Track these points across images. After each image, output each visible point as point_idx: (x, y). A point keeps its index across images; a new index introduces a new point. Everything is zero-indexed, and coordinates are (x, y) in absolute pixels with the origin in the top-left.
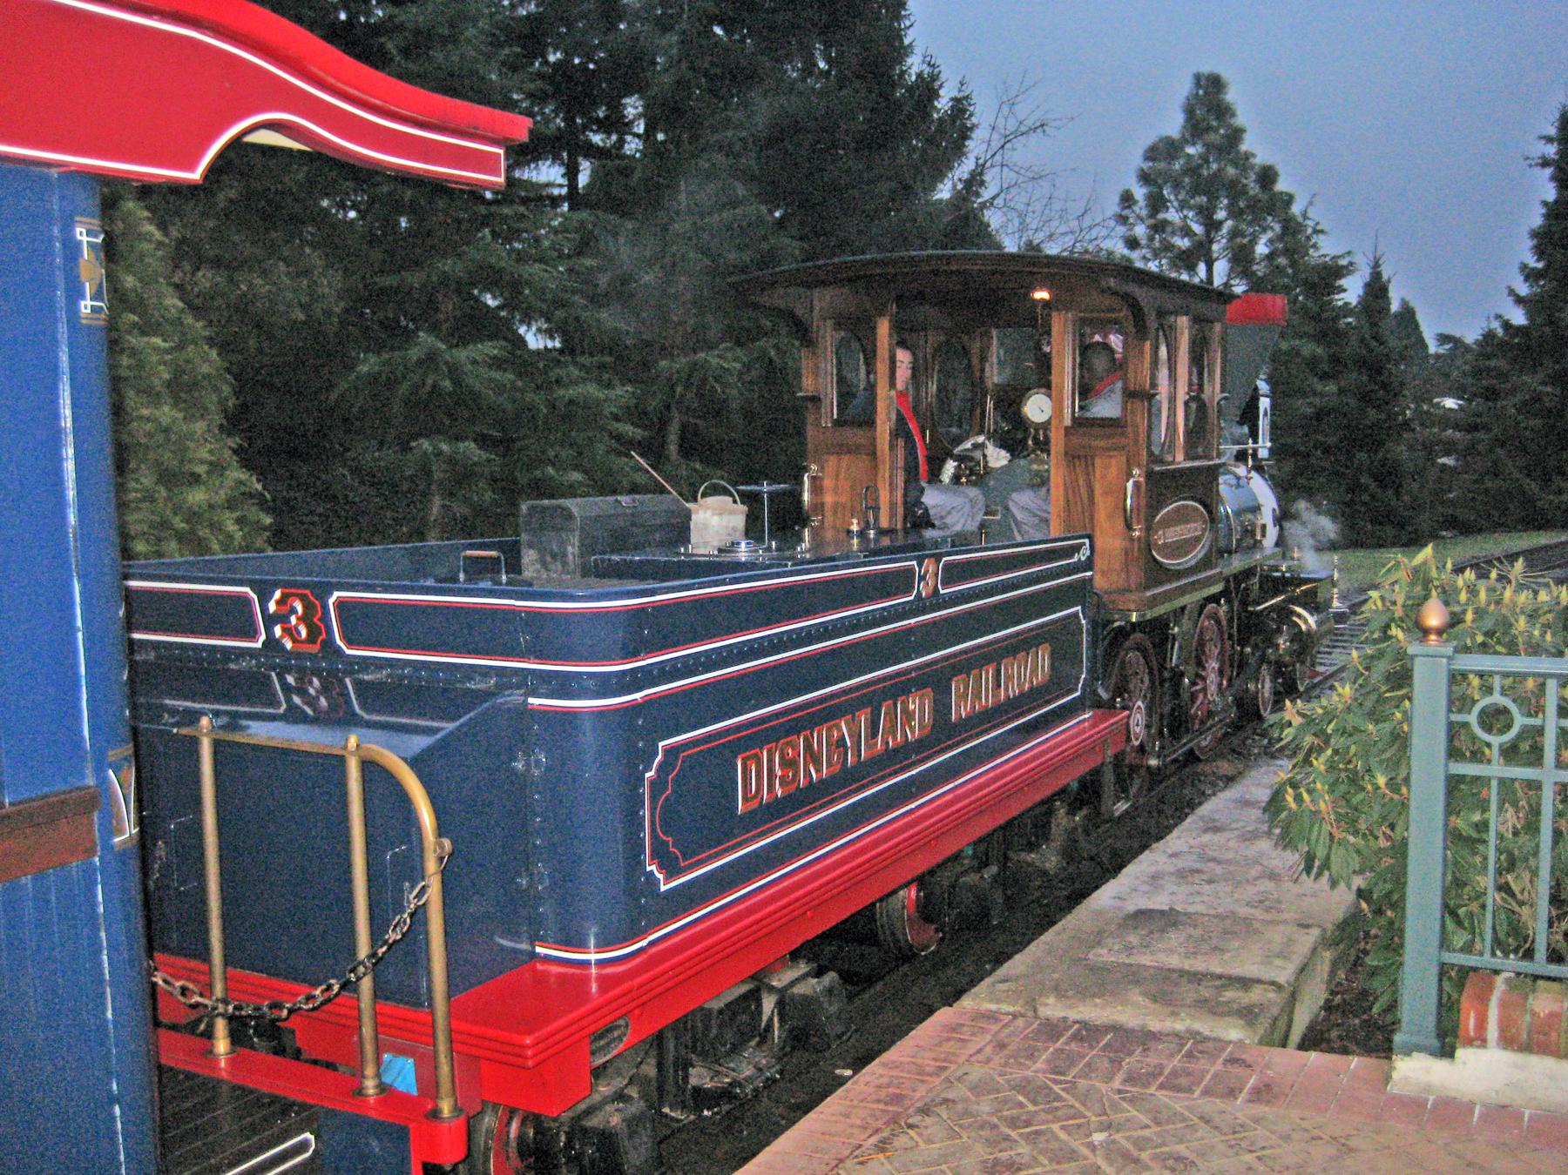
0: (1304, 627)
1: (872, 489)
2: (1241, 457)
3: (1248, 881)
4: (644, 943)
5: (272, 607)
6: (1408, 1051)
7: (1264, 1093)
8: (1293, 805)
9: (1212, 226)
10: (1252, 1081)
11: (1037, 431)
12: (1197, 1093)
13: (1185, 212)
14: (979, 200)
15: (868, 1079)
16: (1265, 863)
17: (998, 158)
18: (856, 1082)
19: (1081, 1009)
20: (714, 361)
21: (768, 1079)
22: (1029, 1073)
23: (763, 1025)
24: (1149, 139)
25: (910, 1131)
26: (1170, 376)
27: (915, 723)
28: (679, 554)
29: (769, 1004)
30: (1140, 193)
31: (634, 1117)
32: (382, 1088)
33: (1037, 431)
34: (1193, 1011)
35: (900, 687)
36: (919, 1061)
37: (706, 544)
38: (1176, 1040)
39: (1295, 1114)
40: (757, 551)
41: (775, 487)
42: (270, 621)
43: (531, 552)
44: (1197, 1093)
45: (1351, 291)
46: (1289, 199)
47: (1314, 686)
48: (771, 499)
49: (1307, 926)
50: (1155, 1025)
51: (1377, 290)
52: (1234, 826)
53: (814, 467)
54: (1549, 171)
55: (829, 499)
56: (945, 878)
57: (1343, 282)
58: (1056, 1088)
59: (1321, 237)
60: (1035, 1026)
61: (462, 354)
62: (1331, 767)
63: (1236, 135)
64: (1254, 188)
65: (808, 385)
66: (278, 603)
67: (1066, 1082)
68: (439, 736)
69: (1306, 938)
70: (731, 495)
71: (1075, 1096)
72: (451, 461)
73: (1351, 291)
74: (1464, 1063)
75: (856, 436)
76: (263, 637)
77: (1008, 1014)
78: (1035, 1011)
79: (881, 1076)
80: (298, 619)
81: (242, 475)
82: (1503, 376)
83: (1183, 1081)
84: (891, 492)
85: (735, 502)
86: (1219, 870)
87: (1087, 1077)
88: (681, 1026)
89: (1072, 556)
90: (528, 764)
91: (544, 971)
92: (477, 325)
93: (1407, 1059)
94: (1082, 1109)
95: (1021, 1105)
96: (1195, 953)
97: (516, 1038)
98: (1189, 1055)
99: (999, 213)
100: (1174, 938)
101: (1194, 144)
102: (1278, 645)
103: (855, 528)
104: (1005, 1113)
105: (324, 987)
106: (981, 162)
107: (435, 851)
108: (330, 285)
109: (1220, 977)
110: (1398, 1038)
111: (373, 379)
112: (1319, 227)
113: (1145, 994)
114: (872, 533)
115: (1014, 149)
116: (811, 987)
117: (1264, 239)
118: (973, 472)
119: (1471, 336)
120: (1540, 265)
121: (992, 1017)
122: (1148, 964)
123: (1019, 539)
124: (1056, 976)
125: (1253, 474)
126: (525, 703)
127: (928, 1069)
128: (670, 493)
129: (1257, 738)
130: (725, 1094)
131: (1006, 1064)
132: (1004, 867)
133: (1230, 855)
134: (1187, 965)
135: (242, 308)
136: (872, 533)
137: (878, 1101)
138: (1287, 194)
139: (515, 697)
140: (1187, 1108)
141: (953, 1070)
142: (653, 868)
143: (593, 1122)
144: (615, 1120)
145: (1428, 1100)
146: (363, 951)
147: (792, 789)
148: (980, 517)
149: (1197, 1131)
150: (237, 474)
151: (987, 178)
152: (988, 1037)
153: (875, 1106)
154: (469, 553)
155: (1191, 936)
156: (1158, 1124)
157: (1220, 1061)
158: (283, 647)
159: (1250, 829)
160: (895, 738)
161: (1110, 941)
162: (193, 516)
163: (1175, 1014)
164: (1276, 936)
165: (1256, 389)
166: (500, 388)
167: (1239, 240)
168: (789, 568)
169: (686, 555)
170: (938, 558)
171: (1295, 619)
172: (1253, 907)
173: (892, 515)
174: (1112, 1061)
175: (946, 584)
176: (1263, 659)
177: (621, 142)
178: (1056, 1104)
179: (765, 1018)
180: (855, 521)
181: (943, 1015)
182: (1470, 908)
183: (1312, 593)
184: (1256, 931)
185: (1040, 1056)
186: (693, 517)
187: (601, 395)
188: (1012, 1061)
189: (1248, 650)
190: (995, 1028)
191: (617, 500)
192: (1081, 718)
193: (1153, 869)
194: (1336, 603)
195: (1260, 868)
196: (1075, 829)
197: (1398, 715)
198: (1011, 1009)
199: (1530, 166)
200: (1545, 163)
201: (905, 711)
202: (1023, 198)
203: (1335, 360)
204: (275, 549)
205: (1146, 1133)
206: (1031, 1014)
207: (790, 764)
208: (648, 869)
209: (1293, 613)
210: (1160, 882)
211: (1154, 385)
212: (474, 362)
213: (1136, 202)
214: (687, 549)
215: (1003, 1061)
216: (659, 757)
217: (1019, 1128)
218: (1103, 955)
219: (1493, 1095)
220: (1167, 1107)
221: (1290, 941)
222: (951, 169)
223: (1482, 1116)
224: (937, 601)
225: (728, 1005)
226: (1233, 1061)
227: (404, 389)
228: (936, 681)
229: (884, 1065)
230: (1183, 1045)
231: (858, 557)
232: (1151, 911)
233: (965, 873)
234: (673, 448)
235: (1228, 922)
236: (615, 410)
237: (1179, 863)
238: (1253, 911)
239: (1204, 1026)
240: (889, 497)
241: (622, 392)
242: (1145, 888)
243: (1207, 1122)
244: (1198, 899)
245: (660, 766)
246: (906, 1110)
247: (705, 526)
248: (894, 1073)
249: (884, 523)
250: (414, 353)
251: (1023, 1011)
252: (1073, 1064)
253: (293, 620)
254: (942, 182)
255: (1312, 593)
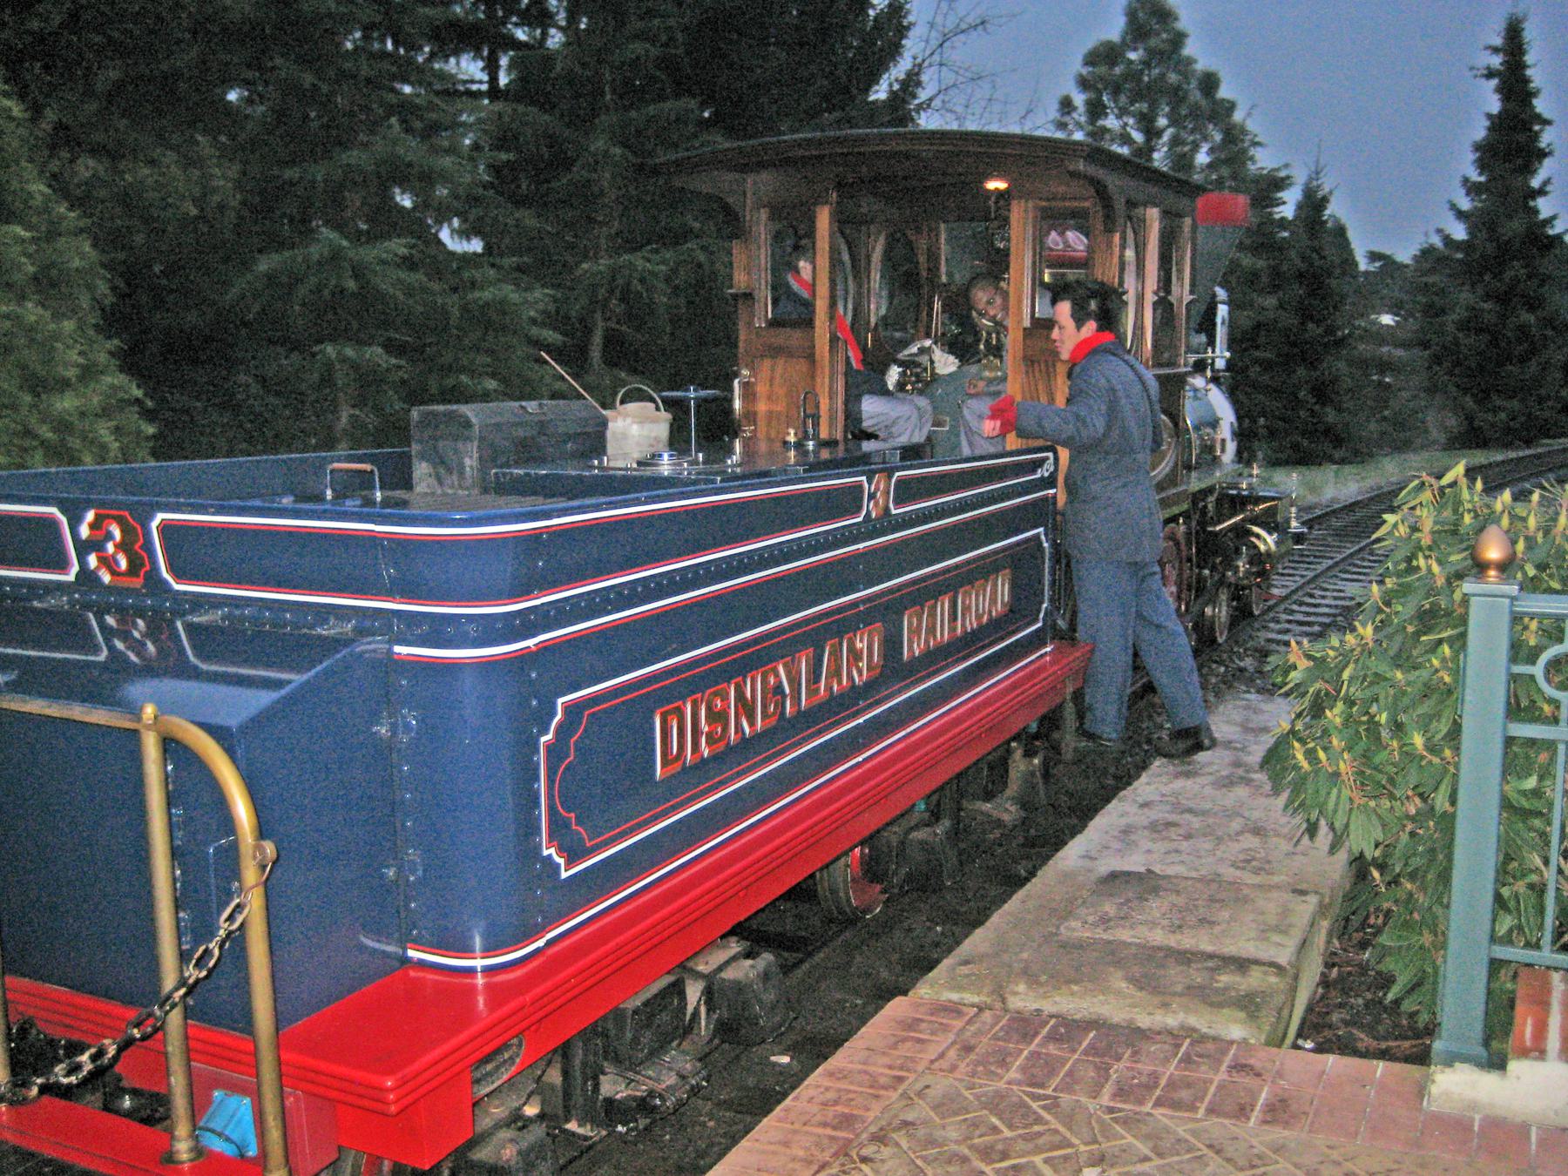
0: (1262, 548)
1: (811, 395)
2: (1200, 367)
3: (1229, 835)
4: (541, 943)
5: (84, 531)
6: (1450, 1060)
7: (1278, 1111)
8: (1305, 765)
9: (1152, 133)
10: (1264, 1095)
11: (989, 334)
12: (1201, 1113)
13: (1125, 119)
14: (916, 102)
15: (812, 1092)
16: (1247, 814)
17: (936, 58)
18: (796, 1098)
19: (1057, 999)
20: (640, 263)
21: (692, 1087)
22: (1002, 1085)
23: (688, 1018)
24: (1089, 43)
25: (863, 1167)
26: (1138, 275)
27: (863, 664)
28: (594, 467)
29: (694, 992)
30: (1079, 99)
31: (531, 1149)
32: (198, 1150)
33: (989, 334)
34: (1185, 1000)
35: (842, 625)
36: (871, 1069)
37: (625, 456)
38: (1169, 1039)
39: (1320, 1140)
40: (681, 465)
41: (703, 393)
42: (83, 548)
43: (424, 465)
44: (1201, 1113)
45: (1287, 208)
46: (1231, 107)
47: (1270, 609)
48: (698, 406)
49: (1303, 893)
50: (1144, 1021)
51: (1314, 204)
52: (1207, 770)
53: (745, 372)
54: (1494, 82)
55: (762, 407)
56: (893, 836)
57: (1283, 195)
58: (1035, 1105)
59: (1259, 149)
60: (1004, 1022)
61: (369, 254)
62: (1348, 720)
63: (1179, 39)
64: (1196, 96)
65: (741, 280)
66: (92, 526)
67: (1046, 1097)
68: (288, 689)
69: (1302, 907)
70: (652, 400)
71: (1056, 1116)
72: (355, 367)
73: (1287, 208)
74: (1518, 1078)
75: (794, 337)
76: (75, 568)
77: (973, 1006)
78: (1004, 1001)
79: (827, 1089)
80: (116, 546)
81: (120, 379)
82: (1442, 292)
83: (1184, 1094)
84: (831, 398)
85: (658, 409)
86: (1196, 822)
87: (1071, 1091)
88: (594, 1031)
89: (1034, 471)
90: (394, 729)
91: (418, 979)
92: (386, 220)
93: (1447, 1070)
94: (1068, 1135)
95: (995, 1130)
96: (1180, 927)
97: (374, 1079)
98: (1187, 1059)
99: (936, 114)
100: (1156, 907)
101: (1135, 49)
102: (1238, 567)
103: (792, 438)
104: (976, 1141)
105: (93, 1050)
106: (919, 61)
107: (255, 857)
108: (224, 178)
109: (1211, 956)
110: (1438, 1046)
111: (271, 278)
112: (1257, 140)
113: (1132, 980)
114: (811, 445)
115: (953, 48)
116: (745, 971)
117: (1205, 148)
118: (920, 380)
119: (1405, 255)
120: (1482, 179)
121: (954, 1009)
122: (1129, 940)
123: (966, 452)
124: (1025, 955)
125: (1211, 386)
126: (390, 651)
127: (882, 1080)
128: (585, 398)
129: (1214, 666)
130: (643, 1105)
131: (974, 1074)
132: (957, 820)
133: (1208, 806)
134: (1172, 941)
135: (126, 200)
136: (811, 445)
137: (825, 1125)
138: (1228, 101)
139: (373, 645)
140: (1193, 1132)
141: (913, 1083)
142: (552, 851)
143: (482, 1154)
144: (509, 1154)
145: (1472, 1120)
146: (169, 981)
147: (721, 747)
148: (928, 428)
149: (1207, 1165)
150: (115, 378)
151: (924, 78)
152: (951, 1037)
153: (820, 1131)
154: (336, 465)
155: (1174, 905)
156: (1160, 1155)
157: (1224, 1068)
158: (98, 580)
159: (1224, 773)
160: (840, 683)
161: (1082, 911)
162: (63, 426)
163: (1165, 1005)
164: (1270, 906)
165: (1214, 295)
166: (409, 292)
167: (1179, 149)
168: (719, 484)
169: (600, 468)
170: (889, 472)
171: (1254, 539)
172: (1238, 868)
173: (831, 425)
174: (1097, 1068)
175: (898, 503)
176: (1222, 582)
177: (545, 35)
178: (1036, 1128)
179: (690, 1009)
180: (792, 432)
181: (896, 1007)
182: (1515, 888)
183: (1272, 512)
184: (1246, 900)
185: (1012, 1063)
186: (610, 425)
187: (515, 297)
188: (980, 1068)
189: (1207, 572)
190: (958, 1024)
191: (522, 407)
192: (1043, 651)
193: (1123, 821)
194: (1294, 524)
195: (1240, 820)
196: (1033, 774)
197: (1435, 662)
198: (976, 999)
199: (1476, 76)
200: (1490, 74)
201: (851, 648)
202: (962, 100)
203: (1276, 273)
204: (157, 459)
205: (1146, 1167)
206: (998, 1005)
207: (718, 717)
208: (546, 853)
209: (1250, 533)
210: (1133, 837)
211: (1121, 283)
212: (383, 262)
213: (1075, 109)
214: (601, 462)
215: (969, 1069)
216: (559, 716)
217: (994, 1161)
218: (1075, 929)
219: (1552, 1114)
220: (1167, 1130)
221: (1285, 912)
222: (887, 69)
223: (1541, 1142)
224: (887, 523)
225: (646, 1004)
226: (1239, 1067)
227: (302, 291)
228: (888, 611)
229: (831, 1074)
230: (1178, 1046)
231: (797, 472)
232: (1129, 874)
233: (916, 827)
234: (596, 354)
235: (1215, 886)
236: (532, 313)
237: (1155, 814)
238: (1238, 873)
239: (1201, 1021)
240: (829, 403)
241: (540, 297)
242: (1116, 845)
243: (1218, 1152)
244: (1175, 857)
245: (560, 726)
246: (857, 1136)
247: (625, 436)
248: (843, 1085)
249: (824, 434)
250: (315, 251)
251: (989, 1000)
252: (1052, 1072)
253: (110, 548)
254: (878, 83)
255: (1272, 512)
